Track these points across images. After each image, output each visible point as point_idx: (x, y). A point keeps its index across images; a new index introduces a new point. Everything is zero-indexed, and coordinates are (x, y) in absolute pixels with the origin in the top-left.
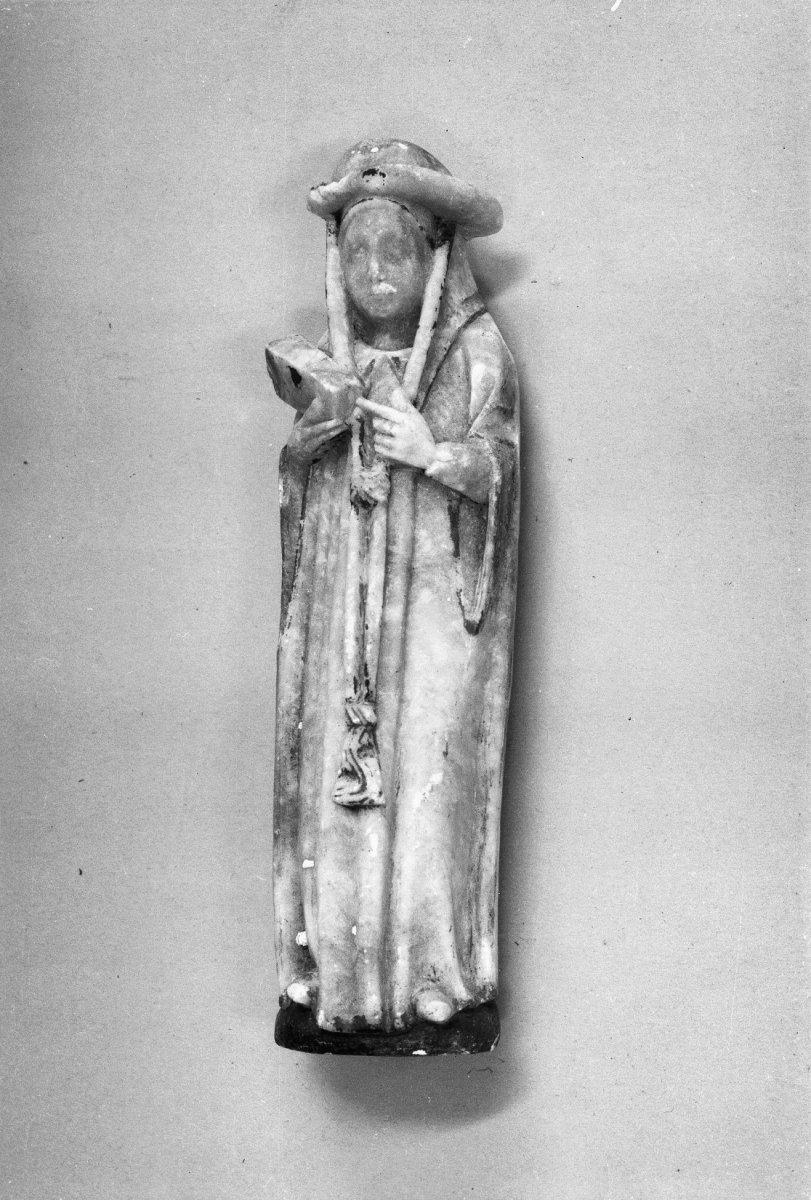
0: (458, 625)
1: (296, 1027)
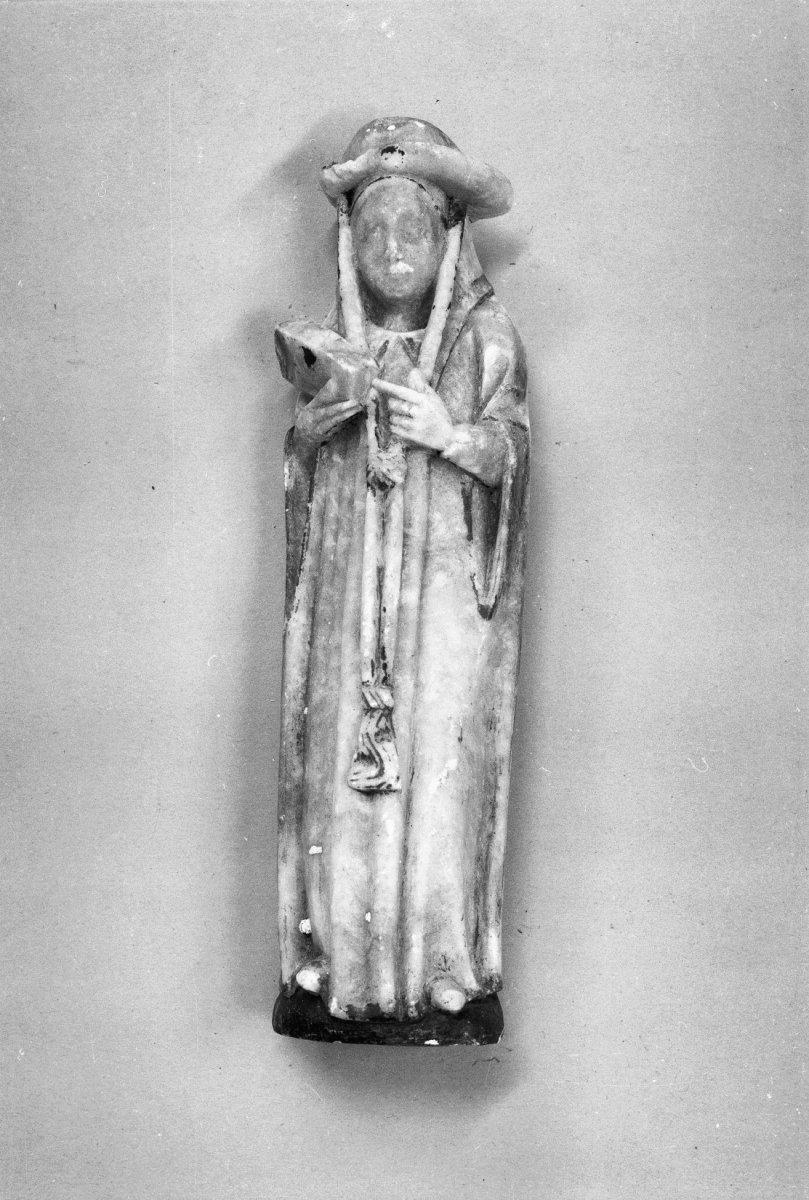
0: (472, 609)
1: (301, 1017)
